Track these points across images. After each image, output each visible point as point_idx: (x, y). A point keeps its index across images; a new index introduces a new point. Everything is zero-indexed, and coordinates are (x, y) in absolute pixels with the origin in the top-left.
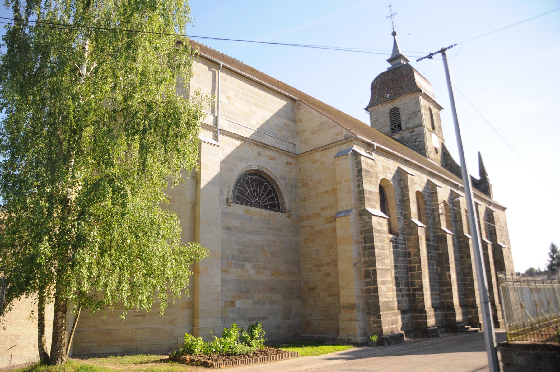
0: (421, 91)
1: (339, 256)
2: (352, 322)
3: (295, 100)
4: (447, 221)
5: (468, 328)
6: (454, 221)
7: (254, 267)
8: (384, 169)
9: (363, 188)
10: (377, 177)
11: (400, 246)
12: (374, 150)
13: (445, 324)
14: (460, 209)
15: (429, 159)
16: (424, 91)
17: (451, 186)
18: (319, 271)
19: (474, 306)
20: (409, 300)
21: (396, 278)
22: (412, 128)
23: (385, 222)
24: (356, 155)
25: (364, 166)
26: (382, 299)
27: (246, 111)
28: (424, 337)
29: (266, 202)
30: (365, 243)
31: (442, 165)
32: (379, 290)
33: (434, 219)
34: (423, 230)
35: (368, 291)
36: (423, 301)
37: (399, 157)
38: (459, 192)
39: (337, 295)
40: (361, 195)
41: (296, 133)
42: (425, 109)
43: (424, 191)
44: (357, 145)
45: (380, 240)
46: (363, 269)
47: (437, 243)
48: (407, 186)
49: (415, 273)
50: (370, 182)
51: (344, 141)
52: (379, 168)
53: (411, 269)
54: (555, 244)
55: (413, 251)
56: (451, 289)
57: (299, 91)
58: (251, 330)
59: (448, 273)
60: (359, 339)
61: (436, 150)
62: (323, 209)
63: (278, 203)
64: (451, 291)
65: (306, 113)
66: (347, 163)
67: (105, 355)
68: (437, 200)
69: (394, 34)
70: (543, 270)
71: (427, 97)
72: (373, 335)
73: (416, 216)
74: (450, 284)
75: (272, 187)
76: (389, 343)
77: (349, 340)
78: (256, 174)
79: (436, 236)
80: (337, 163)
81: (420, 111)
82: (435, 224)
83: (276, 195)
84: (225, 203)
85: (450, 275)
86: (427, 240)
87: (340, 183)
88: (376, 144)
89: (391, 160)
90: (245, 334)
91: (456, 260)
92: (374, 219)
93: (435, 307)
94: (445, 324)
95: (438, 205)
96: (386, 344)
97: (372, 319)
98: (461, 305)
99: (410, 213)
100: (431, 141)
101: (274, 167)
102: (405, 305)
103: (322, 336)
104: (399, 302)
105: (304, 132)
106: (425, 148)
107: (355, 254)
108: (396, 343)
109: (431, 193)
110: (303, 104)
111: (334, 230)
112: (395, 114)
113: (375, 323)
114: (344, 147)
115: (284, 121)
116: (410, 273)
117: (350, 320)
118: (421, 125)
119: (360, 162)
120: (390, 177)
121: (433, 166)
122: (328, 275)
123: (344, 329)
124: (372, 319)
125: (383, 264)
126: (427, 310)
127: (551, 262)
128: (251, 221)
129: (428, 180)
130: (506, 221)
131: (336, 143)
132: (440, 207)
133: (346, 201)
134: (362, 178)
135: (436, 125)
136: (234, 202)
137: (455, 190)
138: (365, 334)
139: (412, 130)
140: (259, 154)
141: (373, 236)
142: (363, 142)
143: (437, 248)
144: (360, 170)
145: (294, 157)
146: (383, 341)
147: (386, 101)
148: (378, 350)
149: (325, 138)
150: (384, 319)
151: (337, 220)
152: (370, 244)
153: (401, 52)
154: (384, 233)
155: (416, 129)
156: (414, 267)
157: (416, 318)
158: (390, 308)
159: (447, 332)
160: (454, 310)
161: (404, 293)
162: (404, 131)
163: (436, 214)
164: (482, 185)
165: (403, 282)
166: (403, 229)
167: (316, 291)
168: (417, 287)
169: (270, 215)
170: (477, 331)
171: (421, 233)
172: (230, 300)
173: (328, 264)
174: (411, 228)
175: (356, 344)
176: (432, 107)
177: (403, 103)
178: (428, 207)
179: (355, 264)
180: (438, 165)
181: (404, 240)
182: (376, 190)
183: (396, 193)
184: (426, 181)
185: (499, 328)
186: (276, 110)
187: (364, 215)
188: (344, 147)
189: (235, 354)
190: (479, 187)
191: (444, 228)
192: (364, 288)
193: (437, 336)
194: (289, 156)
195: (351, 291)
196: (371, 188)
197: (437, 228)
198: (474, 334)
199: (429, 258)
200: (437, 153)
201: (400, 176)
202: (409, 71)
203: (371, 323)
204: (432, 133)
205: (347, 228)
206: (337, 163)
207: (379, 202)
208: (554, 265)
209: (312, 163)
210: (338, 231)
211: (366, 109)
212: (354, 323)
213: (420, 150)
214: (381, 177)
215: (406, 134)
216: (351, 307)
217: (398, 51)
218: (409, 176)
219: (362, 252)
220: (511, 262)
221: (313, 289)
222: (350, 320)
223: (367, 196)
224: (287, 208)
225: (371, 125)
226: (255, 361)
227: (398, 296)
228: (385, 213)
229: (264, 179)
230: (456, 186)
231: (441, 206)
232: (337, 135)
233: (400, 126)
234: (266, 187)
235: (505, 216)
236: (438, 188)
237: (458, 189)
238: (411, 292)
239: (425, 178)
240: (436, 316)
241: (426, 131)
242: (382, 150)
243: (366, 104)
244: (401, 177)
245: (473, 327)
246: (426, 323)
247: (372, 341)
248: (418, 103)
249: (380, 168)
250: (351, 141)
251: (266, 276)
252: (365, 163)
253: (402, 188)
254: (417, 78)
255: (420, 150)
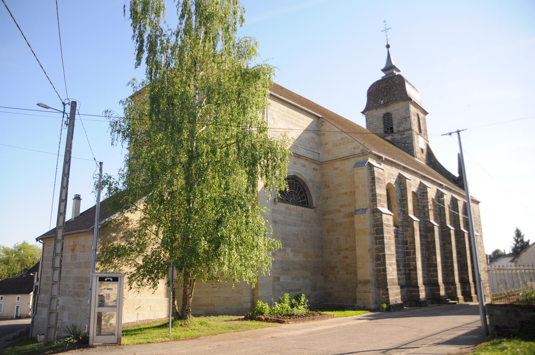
0: (411, 100)
1: (357, 244)
2: (367, 294)
3: (319, 118)
4: (435, 215)
5: (448, 301)
6: (439, 215)
7: (292, 251)
8: (389, 175)
9: (375, 192)
10: (385, 182)
11: (400, 236)
12: (382, 161)
13: (431, 297)
14: (444, 205)
15: (416, 159)
16: (413, 99)
17: (437, 186)
18: (339, 254)
19: (454, 284)
20: (406, 278)
21: (397, 261)
22: (402, 131)
23: (391, 218)
24: (371, 166)
25: (376, 175)
26: (389, 277)
27: (284, 127)
28: (417, 306)
29: (299, 200)
30: (377, 234)
31: (427, 164)
32: (387, 270)
33: (424, 213)
34: (418, 223)
35: (378, 271)
36: (416, 279)
37: (400, 165)
38: (443, 191)
39: (355, 273)
40: (374, 197)
41: (320, 145)
42: (414, 115)
43: (417, 191)
44: (371, 158)
45: (388, 232)
46: (375, 254)
47: (426, 232)
48: (406, 189)
49: (411, 257)
50: (380, 187)
51: (361, 154)
52: (386, 175)
53: (408, 254)
54: (520, 228)
55: (409, 240)
56: (437, 270)
57: (315, 104)
58: (298, 298)
59: (434, 257)
60: (372, 307)
61: (422, 150)
62: (342, 206)
63: (307, 201)
64: (436, 271)
65: (327, 126)
66: (364, 172)
67: (216, 314)
68: (427, 199)
69: (388, 46)
70: (507, 252)
71: (416, 105)
72: (383, 303)
73: (412, 212)
74: (436, 266)
75: (303, 188)
76: (394, 310)
77: (364, 307)
78: (292, 179)
79: (426, 227)
80: (355, 172)
81: (409, 117)
82: (425, 218)
83: (306, 194)
84: (273, 202)
85: (436, 259)
86: (420, 231)
87: (358, 187)
88: (384, 156)
89: (394, 168)
90: (294, 301)
91: (441, 246)
92: (384, 216)
93: (425, 284)
94: (431, 297)
95: (428, 202)
96: (392, 310)
97: (382, 292)
98: (444, 282)
99: (408, 210)
100: (418, 143)
101: (306, 173)
102: (403, 282)
103: (341, 304)
104: (399, 279)
105: (327, 144)
106: (413, 149)
107: (369, 243)
108: (399, 310)
109: (423, 193)
110: (326, 122)
111: (353, 223)
112: (387, 118)
113: (383, 294)
114: (361, 159)
115: (311, 135)
116: (407, 257)
117: (365, 292)
118: (410, 129)
119: (374, 172)
120: (393, 181)
121: (418, 165)
122: (347, 257)
123: (360, 299)
124: (382, 292)
125: (390, 250)
126: (419, 285)
127: (516, 245)
128: (290, 215)
129: (421, 182)
130: (479, 213)
131: (354, 156)
132: (429, 204)
133: (363, 202)
134: (375, 184)
135: (422, 128)
136: (279, 201)
137: (440, 189)
138: (376, 303)
139: (401, 133)
140: (295, 163)
141: (383, 229)
142: (375, 155)
143: (426, 237)
144: (373, 178)
145: (319, 164)
146: (390, 309)
147: (380, 106)
148: (387, 314)
149: (345, 150)
150: (390, 292)
151: (356, 216)
152: (381, 235)
153: (393, 63)
154: (390, 227)
155: (405, 133)
156: (410, 252)
157: (410, 291)
158: (394, 284)
159: (432, 303)
160: (438, 286)
161: (402, 272)
162: (395, 133)
163: (426, 209)
164: (460, 182)
165: (401, 263)
166: (402, 222)
167: (336, 269)
168: (412, 268)
169: (302, 210)
170: (455, 303)
171: (416, 226)
172: (276, 276)
173: (346, 249)
174: (408, 222)
175: (371, 310)
176: (419, 113)
177: (395, 109)
178: (420, 204)
179: (369, 250)
180: (423, 163)
181: (403, 231)
182: (384, 193)
183: (398, 194)
184: (418, 183)
185: (472, 301)
186: (306, 127)
187: (376, 213)
188: (361, 159)
189: (293, 315)
190: (457, 184)
191: (432, 221)
192: (376, 268)
193: (426, 306)
194: (315, 163)
195: (366, 270)
196: (381, 191)
197: (427, 221)
198: (454, 305)
199: (422, 245)
200: (423, 153)
201: (401, 180)
202: (400, 82)
203: (381, 294)
204: (419, 136)
205: (363, 222)
206: (355, 172)
207: (386, 202)
208: (518, 248)
209: (334, 169)
210: (356, 225)
211: (363, 113)
212: (369, 294)
213: (409, 151)
214: (387, 182)
215: (397, 137)
216: (366, 282)
217: (391, 62)
218: (407, 180)
219: (374, 241)
220: (483, 247)
221: (334, 268)
222: (365, 292)
223: (378, 198)
224: (314, 205)
225: (367, 126)
226: (309, 320)
227: (398, 274)
228: (391, 211)
229: (298, 182)
230: (441, 186)
231: (430, 203)
232: (354, 149)
233: (392, 129)
234: (299, 188)
235: (478, 208)
236: (428, 189)
237: (443, 188)
238: (408, 272)
239: (418, 180)
240: (426, 290)
241: (415, 136)
242: (388, 160)
243: (363, 108)
244: (401, 181)
245: (452, 300)
246: (419, 296)
247: (383, 308)
248: (408, 109)
249: (386, 174)
250: (366, 155)
251: (300, 258)
252: (377, 173)
253: (402, 190)
254: (408, 88)
255: (409, 151)
